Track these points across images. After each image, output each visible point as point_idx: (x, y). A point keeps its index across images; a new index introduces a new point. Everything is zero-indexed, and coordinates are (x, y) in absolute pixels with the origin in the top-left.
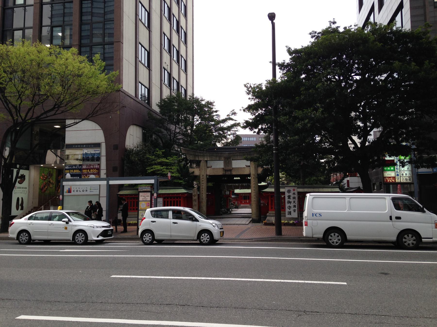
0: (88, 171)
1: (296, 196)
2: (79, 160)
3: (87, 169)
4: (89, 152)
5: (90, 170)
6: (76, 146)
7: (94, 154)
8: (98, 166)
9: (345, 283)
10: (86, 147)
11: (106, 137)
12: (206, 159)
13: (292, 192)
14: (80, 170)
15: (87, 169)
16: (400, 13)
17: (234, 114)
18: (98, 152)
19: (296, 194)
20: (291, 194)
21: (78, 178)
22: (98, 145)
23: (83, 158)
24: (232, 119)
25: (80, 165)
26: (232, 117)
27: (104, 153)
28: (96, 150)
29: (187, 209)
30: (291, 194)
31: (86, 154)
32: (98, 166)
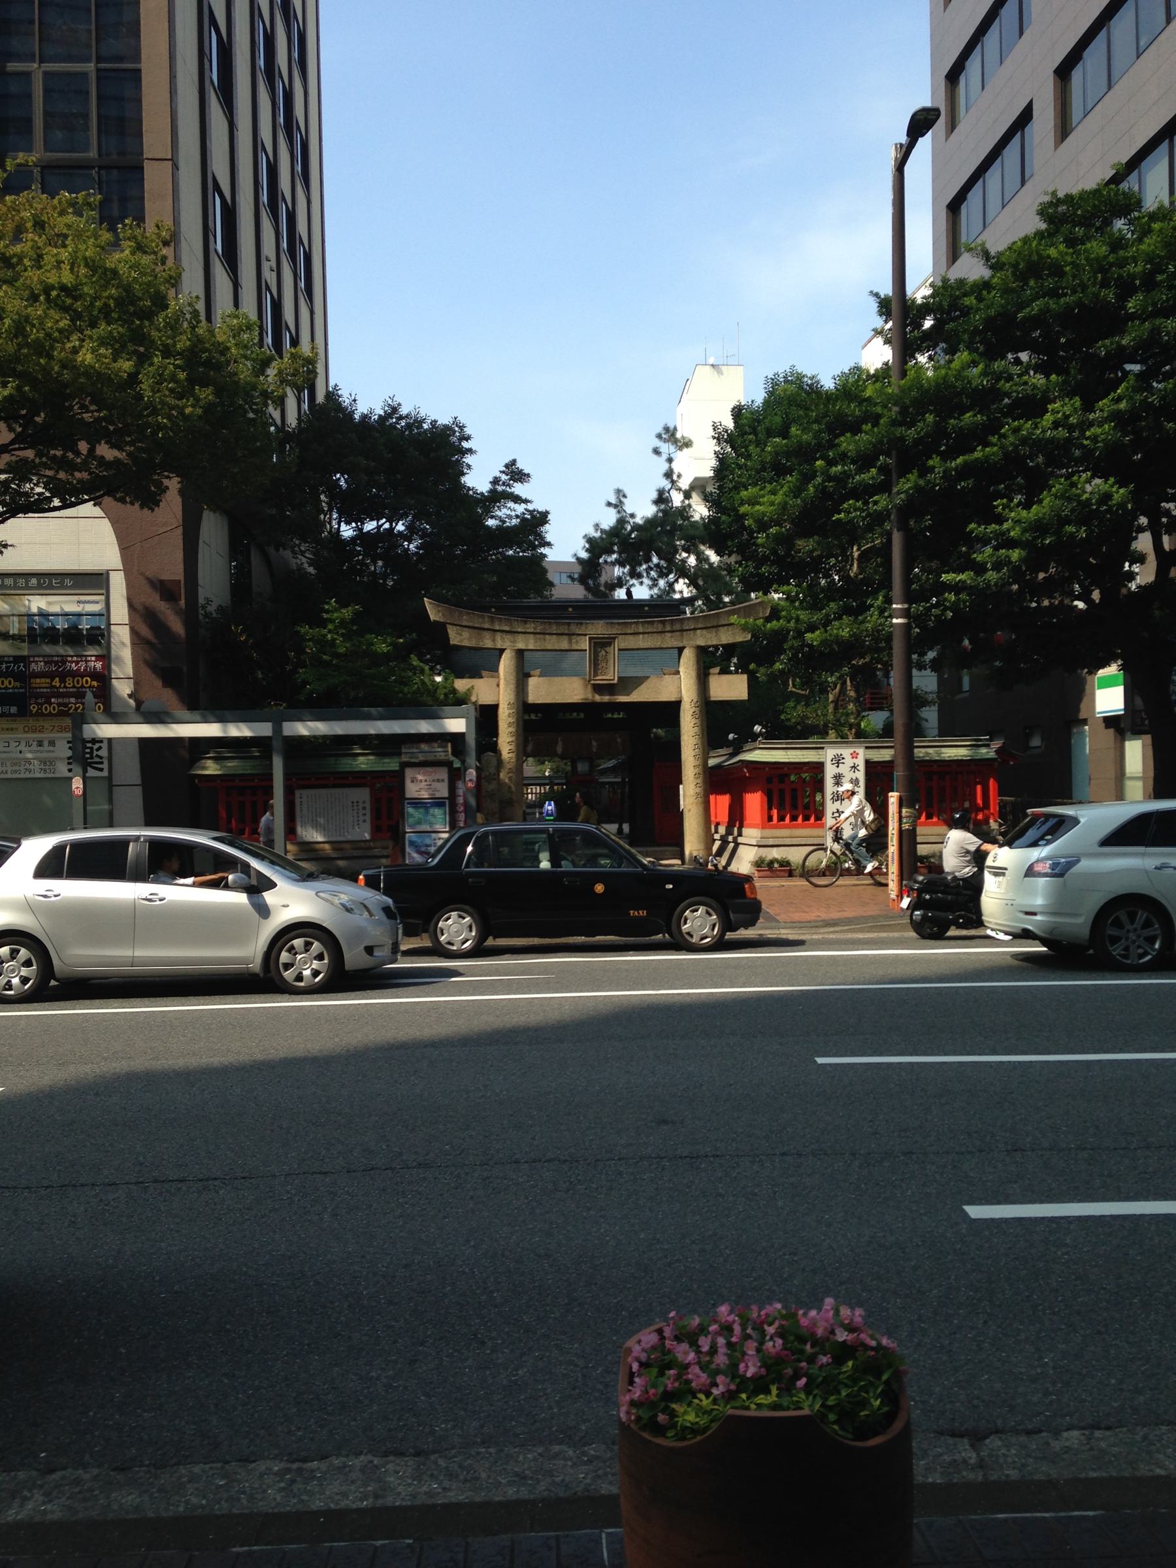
0: (56, 682)
1: (861, 775)
2: (14, 637)
3: (51, 676)
4: (56, 609)
5: (63, 681)
6: (34, 581)
7: (80, 615)
8: (99, 665)
9: (820, 1060)
10: (40, 586)
11: (125, 549)
12: (521, 646)
13: (849, 762)
14: (21, 677)
15: (51, 676)
16: (1018, 135)
17: (519, 476)
18: (96, 608)
19: (862, 767)
20: (844, 769)
21: (14, 710)
22: (95, 581)
23: (31, 629)
24: (517, 499)
25: (18, 659)
26: (518, 489)
27: (120, 612)
28: (83, 598)
29: (202, 838)
30: (844, 769)
31: (43, 614)
32: (99, 665)
